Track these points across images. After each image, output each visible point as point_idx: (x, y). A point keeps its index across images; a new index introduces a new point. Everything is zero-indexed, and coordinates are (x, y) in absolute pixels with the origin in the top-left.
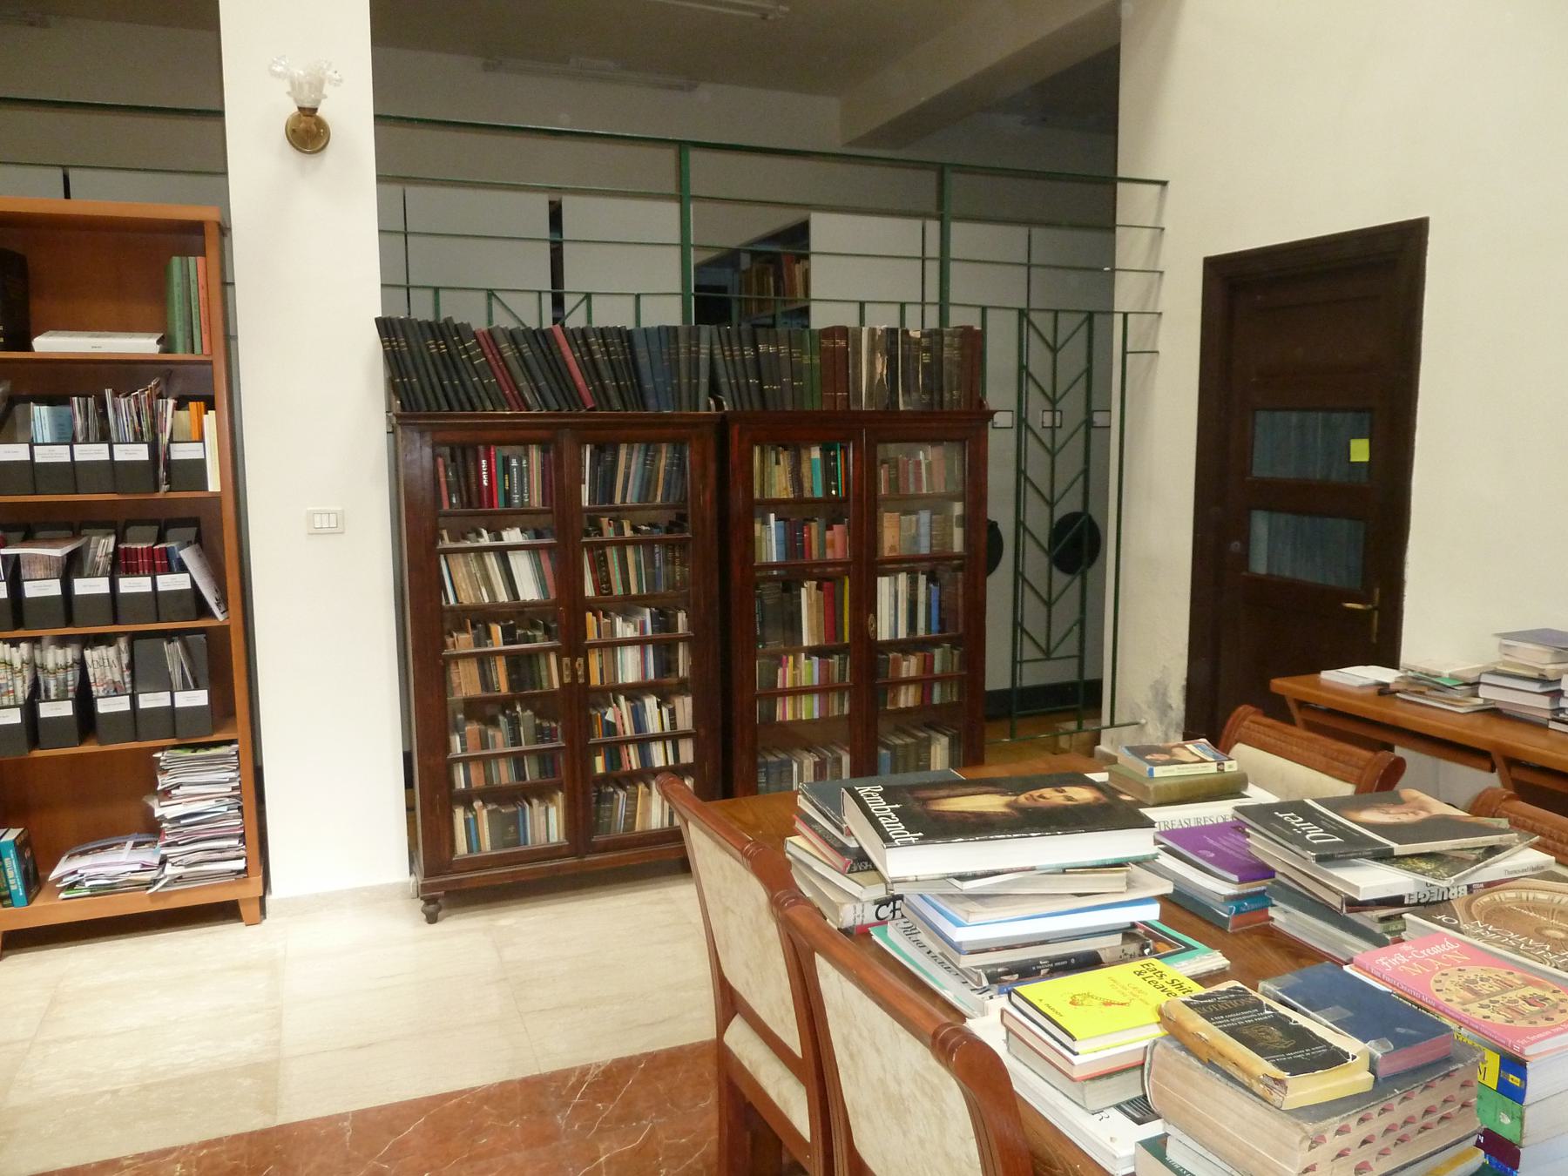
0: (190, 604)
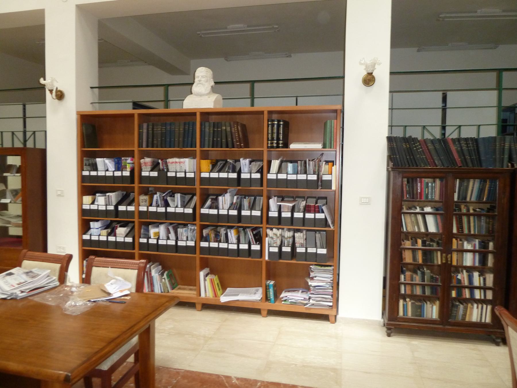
0: (324, 223)
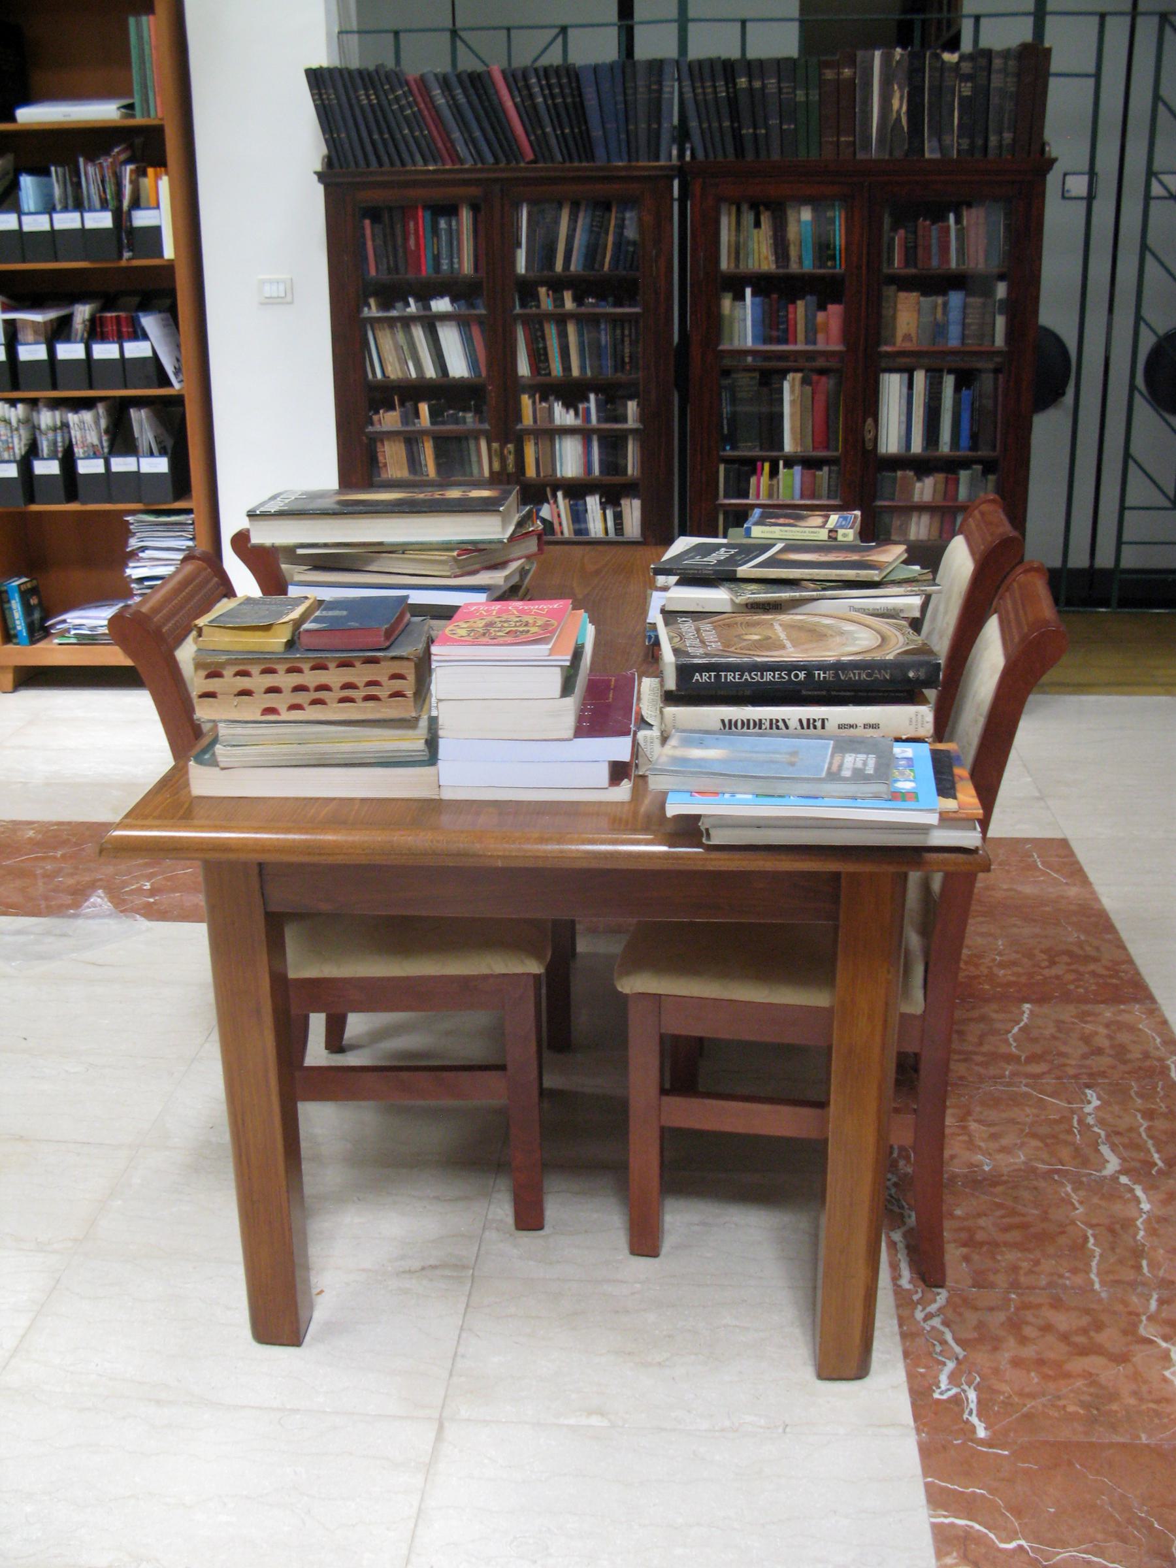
0: (151, 369)
